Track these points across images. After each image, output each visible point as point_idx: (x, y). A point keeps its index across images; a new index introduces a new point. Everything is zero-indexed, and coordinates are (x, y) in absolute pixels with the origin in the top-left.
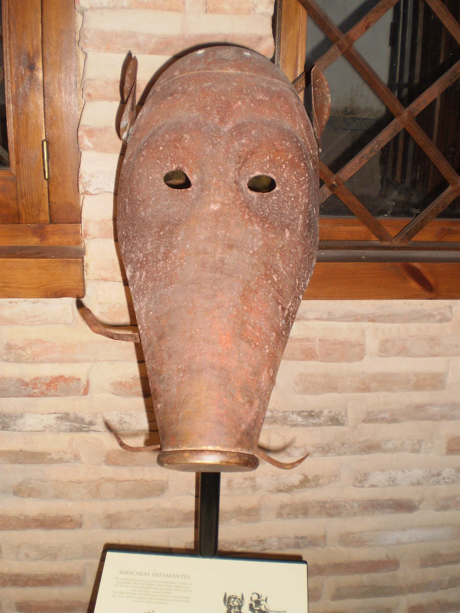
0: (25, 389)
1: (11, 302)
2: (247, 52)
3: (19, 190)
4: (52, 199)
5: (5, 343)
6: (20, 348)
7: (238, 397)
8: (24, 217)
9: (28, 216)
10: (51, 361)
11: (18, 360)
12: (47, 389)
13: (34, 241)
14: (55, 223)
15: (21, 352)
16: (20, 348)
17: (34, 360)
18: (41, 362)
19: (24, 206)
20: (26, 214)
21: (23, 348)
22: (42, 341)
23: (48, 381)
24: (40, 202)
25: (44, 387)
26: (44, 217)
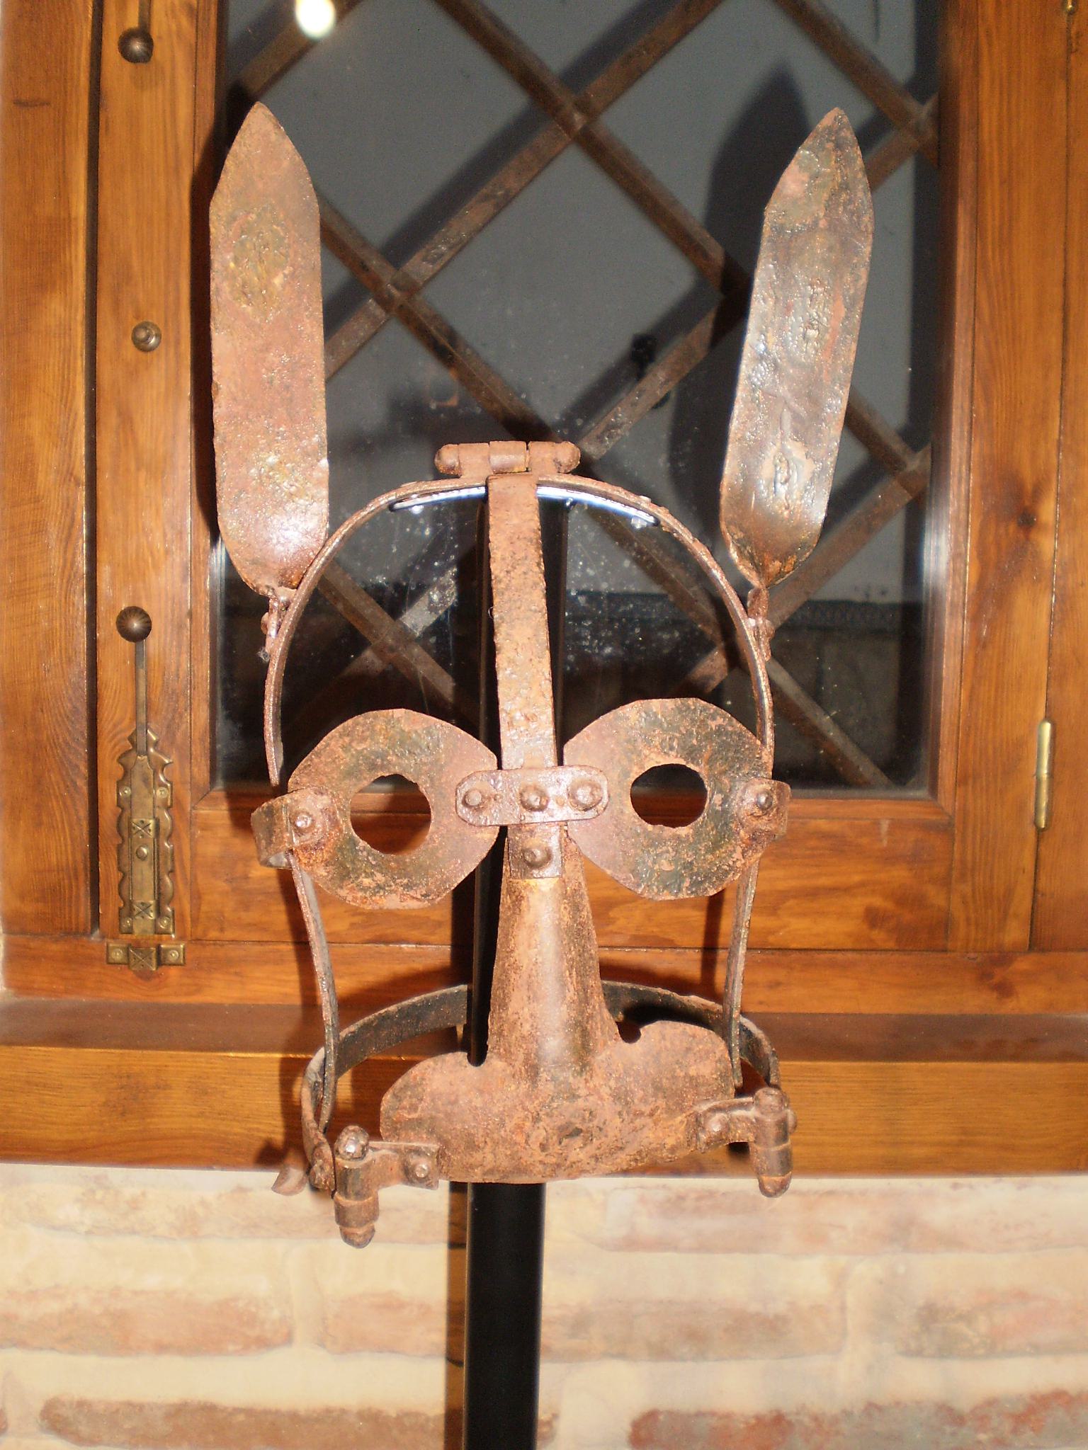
0: (954, 1434)
1: (955, 1186)
2: (166, 885)
3: (957, 856)
4: (1043, 883)
5: (921, 1302)
6: (961, 1317)
7: (314, 1125)
8: (962, 932)
9: (973, 928)
10: (1037, 1350)
11: (948, 1349)
12: (1015, 1431)
13: (126, 993)
14: (1042, 950)
15: (962, 1327)
16: (961, 1317)
17: (994, 1347)
18: (1010, 1353)
19: (965, 903)
20: (969, 924)
21: (967, 1318)
22: (1022, 1295)
23: (1021, 1408)
24: (1009, 893)
25: (1007, 1426)
26: (1015, 933)
